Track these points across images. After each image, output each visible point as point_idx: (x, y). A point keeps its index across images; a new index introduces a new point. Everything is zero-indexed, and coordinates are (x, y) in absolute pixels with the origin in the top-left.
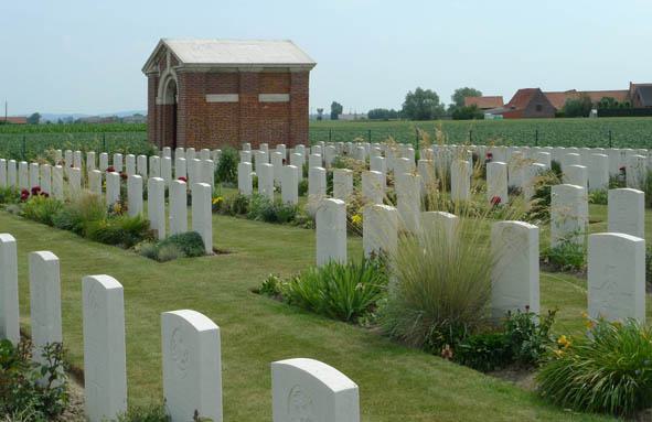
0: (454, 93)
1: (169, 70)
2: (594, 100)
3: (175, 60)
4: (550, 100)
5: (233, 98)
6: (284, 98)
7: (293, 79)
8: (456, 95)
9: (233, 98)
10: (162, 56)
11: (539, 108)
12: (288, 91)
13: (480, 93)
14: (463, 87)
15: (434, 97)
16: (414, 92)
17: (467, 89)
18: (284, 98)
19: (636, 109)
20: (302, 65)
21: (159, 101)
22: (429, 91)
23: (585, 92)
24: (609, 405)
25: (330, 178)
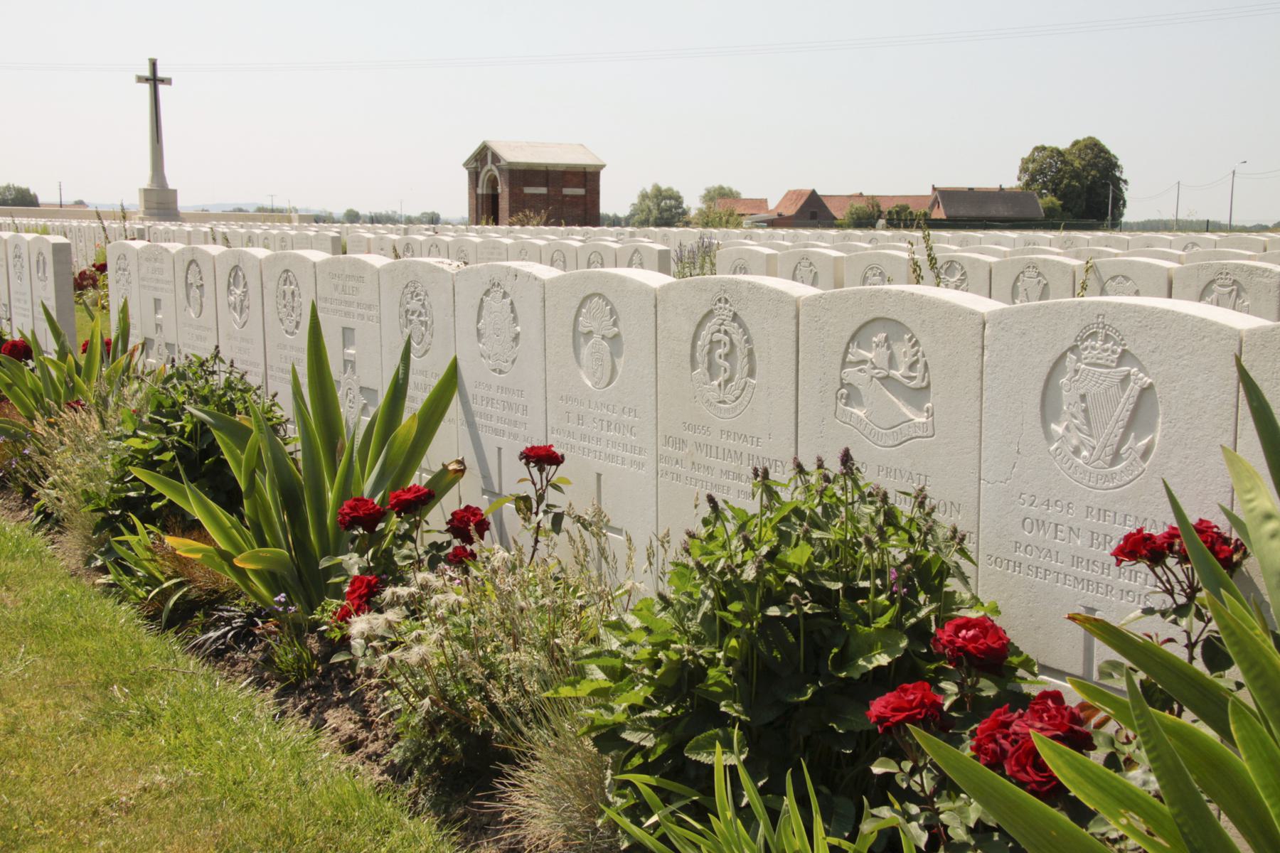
0: (703, 192)
1: (489, 166)
2: (885, 208)
3: (496, 158)
4: (828, 205)
5: (543, 190)
6: (581, 191)
7: (588, 178)
8: (1031, 159)
9: (543, 190)
10: (483, 156)
11: (814, 216)
12: (584, 186)
13: (738, 194)
14: (716, 185)
15: (678, 199)
16: (649, 189)
17: (721, 188)
18: (581, 191)
19: (1121, 190)
20: (595, 166)
21: (480, 191)
22: (670, 189)
23: (873, 197)
24: (1250, 501)
25: (297, 327)
